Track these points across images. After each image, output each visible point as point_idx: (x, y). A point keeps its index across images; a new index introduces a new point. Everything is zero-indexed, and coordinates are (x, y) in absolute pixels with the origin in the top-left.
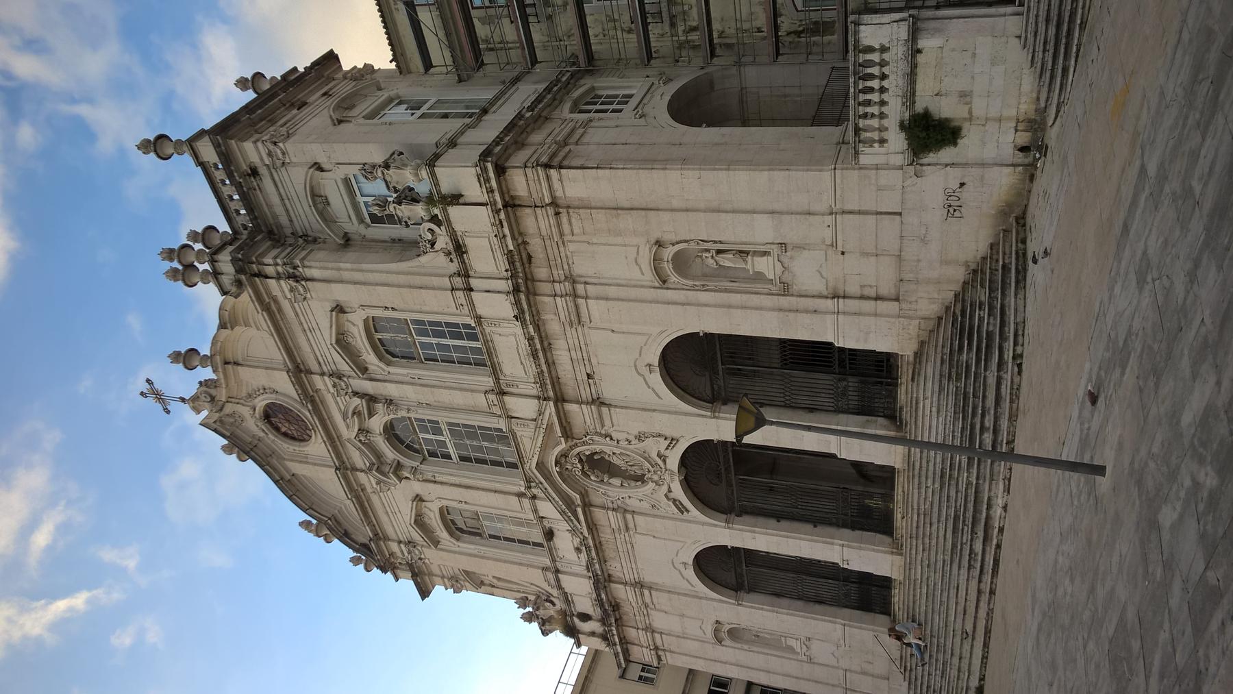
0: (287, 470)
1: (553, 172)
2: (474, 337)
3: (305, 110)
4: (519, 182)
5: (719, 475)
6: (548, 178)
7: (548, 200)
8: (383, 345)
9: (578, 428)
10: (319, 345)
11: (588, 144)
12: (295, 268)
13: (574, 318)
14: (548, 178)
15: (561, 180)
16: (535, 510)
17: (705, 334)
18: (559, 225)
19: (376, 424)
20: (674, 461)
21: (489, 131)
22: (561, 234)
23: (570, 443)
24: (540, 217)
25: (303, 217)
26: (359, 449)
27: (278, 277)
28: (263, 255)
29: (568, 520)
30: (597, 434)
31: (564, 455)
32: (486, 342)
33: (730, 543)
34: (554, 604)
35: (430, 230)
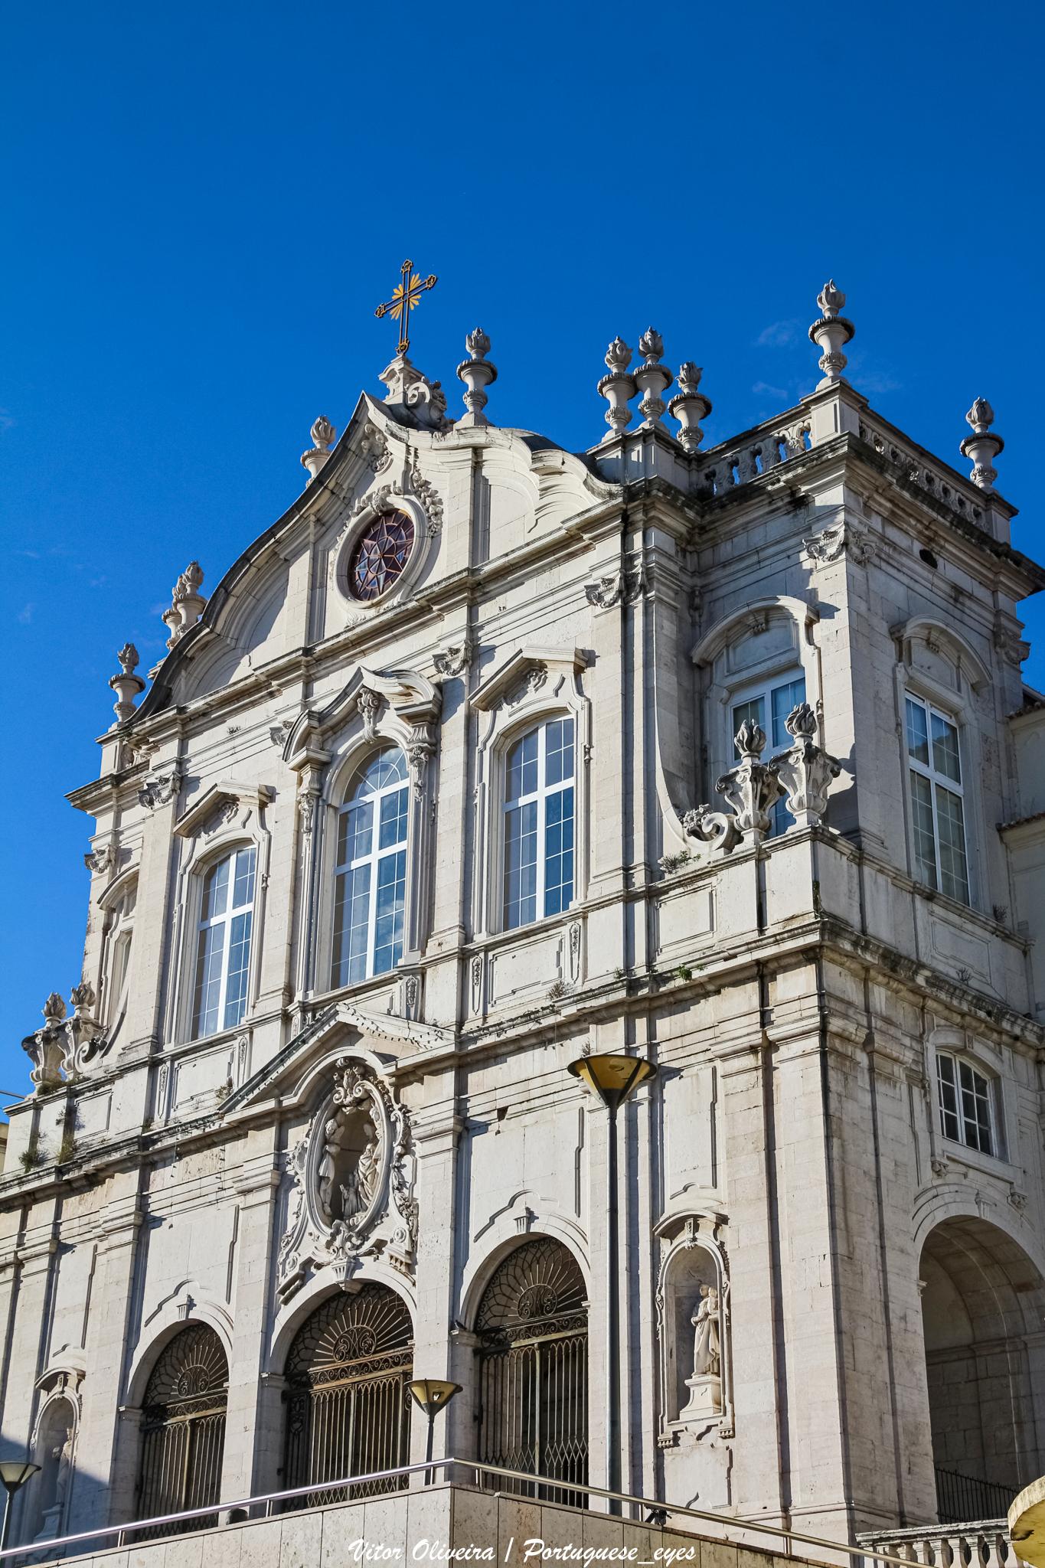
0: (297, 554)
1: (814, 1042)
2: (551, 908)
3: (921, 569)
4: (796, 987)
5: (353, 1354)
6: (805, 1034)
7: (773, 1034)
8: (526, 737)
9: (412, 1094)
10: (516, 626)
11: (873, 1091)
14: (805, 1034)
15: (804, 1055)
16: (263, 1021)
17: (921, 1278)
18: (737, 1053)
19: (391, 725)
20: (372, 1270)
21: (886, 918)
22: (724, 1057)
23: (387, 1081)
24: (745, 1020)
25: (732, 587)
26: (345, 694)
27: (627, 560)
29: (251, 1085)
30: (407, 1129)
31: (368, 1072)
32: (545, 928)
34: (87, 1059)
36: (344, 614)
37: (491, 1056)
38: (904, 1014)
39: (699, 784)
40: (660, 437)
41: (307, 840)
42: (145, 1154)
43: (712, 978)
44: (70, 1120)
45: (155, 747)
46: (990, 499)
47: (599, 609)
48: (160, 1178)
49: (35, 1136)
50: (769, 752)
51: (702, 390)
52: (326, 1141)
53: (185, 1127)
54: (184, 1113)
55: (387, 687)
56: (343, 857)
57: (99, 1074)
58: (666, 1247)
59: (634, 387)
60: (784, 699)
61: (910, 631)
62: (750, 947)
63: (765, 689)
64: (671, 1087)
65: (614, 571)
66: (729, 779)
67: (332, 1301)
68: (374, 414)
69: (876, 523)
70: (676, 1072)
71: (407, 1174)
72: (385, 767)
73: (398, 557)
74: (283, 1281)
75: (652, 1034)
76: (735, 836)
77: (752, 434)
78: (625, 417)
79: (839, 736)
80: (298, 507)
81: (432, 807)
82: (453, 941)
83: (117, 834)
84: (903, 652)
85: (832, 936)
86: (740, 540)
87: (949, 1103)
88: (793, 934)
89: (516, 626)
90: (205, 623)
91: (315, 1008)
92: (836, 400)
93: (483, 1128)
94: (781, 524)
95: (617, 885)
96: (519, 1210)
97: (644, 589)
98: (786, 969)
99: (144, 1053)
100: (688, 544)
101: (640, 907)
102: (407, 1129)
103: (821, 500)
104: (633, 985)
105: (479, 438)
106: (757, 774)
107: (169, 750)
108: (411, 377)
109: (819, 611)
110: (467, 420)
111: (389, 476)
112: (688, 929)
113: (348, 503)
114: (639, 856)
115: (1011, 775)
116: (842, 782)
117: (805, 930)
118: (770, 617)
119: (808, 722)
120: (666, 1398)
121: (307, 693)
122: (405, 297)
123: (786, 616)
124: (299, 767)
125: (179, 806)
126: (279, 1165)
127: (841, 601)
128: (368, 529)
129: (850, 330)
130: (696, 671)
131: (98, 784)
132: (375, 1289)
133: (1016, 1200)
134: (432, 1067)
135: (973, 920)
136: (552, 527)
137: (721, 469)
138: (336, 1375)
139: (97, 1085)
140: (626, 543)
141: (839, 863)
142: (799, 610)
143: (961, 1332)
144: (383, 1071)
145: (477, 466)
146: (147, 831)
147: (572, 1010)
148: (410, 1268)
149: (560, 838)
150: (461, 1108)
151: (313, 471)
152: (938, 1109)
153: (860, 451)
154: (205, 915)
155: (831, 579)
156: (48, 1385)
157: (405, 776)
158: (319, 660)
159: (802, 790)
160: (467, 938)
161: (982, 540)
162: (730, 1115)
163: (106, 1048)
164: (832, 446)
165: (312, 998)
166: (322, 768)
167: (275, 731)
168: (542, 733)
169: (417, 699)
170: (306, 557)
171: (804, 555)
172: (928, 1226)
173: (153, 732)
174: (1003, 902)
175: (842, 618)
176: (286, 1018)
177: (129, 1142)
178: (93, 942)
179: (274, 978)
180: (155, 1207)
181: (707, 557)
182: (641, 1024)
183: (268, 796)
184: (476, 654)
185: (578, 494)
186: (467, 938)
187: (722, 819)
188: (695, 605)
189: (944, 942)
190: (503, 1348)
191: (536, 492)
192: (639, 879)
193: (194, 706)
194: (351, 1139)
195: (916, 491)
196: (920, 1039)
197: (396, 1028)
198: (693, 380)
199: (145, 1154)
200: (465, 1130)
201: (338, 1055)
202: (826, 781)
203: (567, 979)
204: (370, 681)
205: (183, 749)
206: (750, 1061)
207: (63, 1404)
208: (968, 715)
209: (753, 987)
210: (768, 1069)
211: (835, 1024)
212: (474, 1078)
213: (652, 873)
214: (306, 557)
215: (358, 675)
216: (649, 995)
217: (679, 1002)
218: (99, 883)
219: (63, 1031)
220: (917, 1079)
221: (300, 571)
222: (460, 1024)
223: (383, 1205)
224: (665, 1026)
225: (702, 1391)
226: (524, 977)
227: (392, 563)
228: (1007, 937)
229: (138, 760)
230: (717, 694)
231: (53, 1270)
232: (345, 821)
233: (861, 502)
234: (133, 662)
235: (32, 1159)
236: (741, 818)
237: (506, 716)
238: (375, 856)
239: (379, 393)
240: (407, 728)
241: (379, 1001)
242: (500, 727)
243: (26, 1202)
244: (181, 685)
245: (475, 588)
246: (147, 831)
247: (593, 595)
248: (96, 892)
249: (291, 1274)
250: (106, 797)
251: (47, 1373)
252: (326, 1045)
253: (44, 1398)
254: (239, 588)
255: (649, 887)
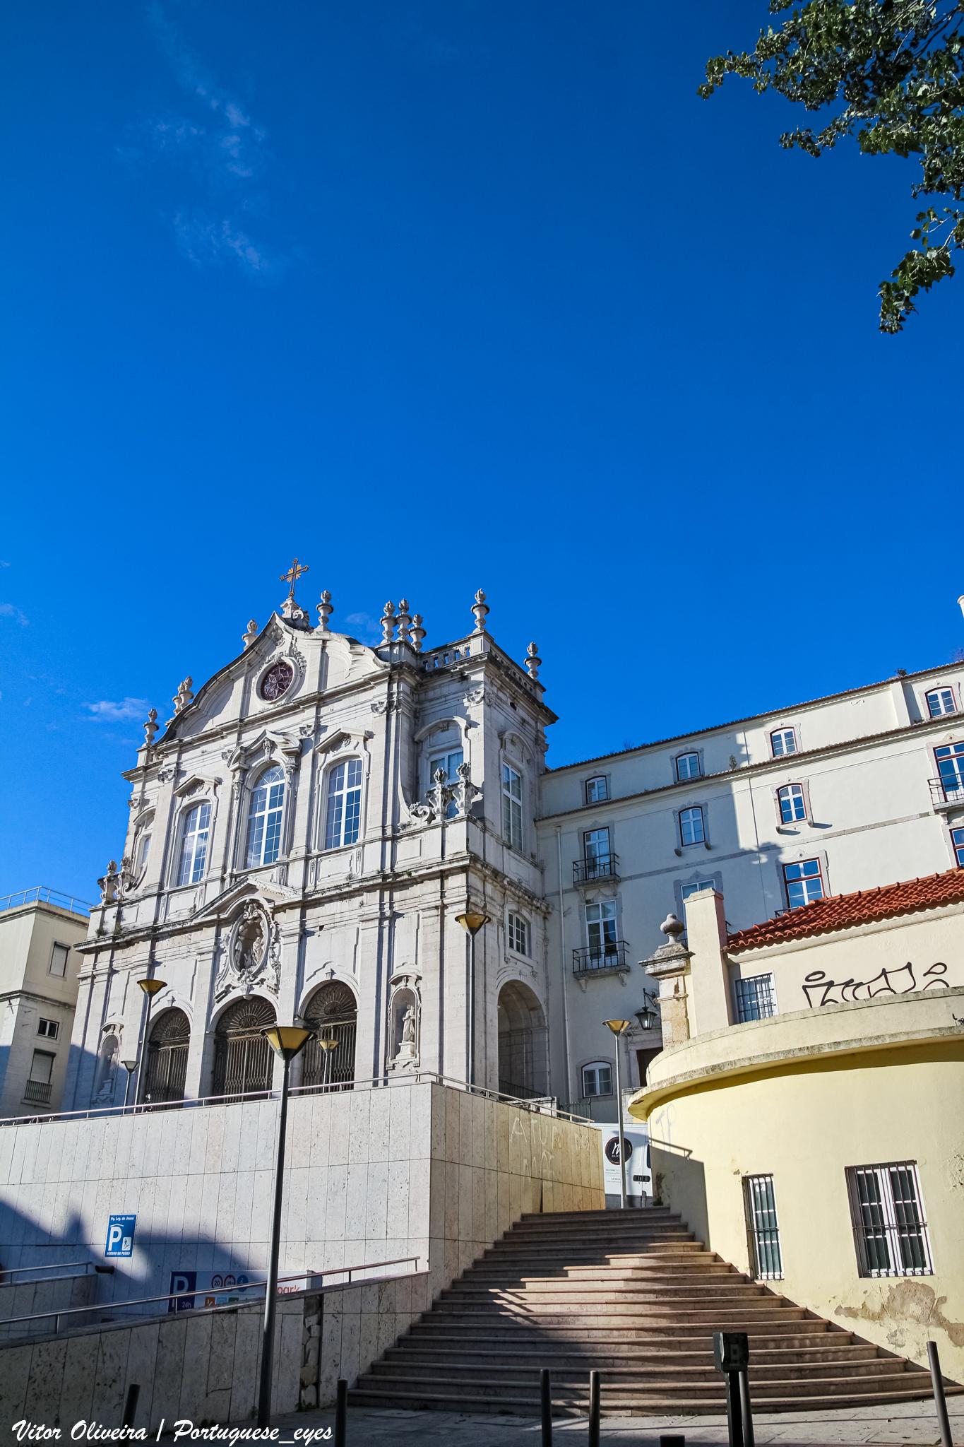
0: (238, 678)
3: (510, 710)
4: (457, 883)
7: (446, 902)
10: (337, 718)
12: (397, 708)
13: (365, 917)
19: (278, 755)
21: (495, 855)
26: (258, 740)
27: (390, 695)
28: (406, 682)
29: (206, 908)
30: (277, 932)
31: (260, 906)
32: (345, 850)
33: (192, 1035)
35: (915, 267)
36: (258, 706)
37: (318, 903)
38: (498, 896)
39: (415, 793)
40: (406, 643)
41: (236, 803)
42: (154, 934)
43: (420, 876)
44: (119, 917)
45: (167, 756)
46: (536, 684)
47: (376, 714)
48: (160, 945)
49: (102, 922)
50: (448, 782)
51: (422, 626)
52: (239, 934)
53: (174, 924)
54: (173, 918)
55: (278, 739)
56: (251, 811)
57: (134, 898)
58: (394, 989)
59: (396, 622)
60: (454, 760)
61: (507, 736)
62: (438, 864)
63: (445, 755)
64: (399, 921)
65: (384, 699)
66: (431, 792)
67: (239, 1003)
68: (278, 621)
69: (495, 689)
70: (401, 915)
71: (276, 951)
72: (273, 774)
73: (285, 684)
74: (217, 993)
75: (391, 898)
76: (432, 817)
77: (445, 647)
78: (390, 634)
79: (477, 778)
80: (241, 657)
81: (295, 793)
82: (302, 852)
83: (143, 792)
84: (503, 745)
85: (474, 863)
86: (438, 691)
87: (511, 934)
88: (458, 860)
89: (337, 718)
90: (194, 704)
91: (236, 876)
92: (482, 638)
93: (312, 933)
94: (455, 686)
95: (379, 834)
96: (328, 969)
97: (397, 708)
98: (453, 874)
99: (155, 890)
100: (415, 690)
101: (389, 844)
102: (277, 932)
103: (473, 678)
104: (385, 877)
105: (326, 636)
106: (444, 791)
107: (173, 758)
108: (295, 607)
109: (471, 724)
110: (320, 628)
111: (281, 650)
112: (409, 855)
113: (263, 658)
114: (389, 822)
115: (540, 798)
116: (478, 797)
117: (463, 859)
118: (449, 724)
119: (466, 770)
120: (390, 1050)
121: (239, 738)
122: (294, 573)
123: (457, 725)
124: (235, 770)
125: (176, 783)
126: (217, 943)
127: (481, 721)
128: (272, 670)
129: (488, 609)
130: (416, 744)
131: (137, 770)
132: (260, 999)
133: (534, 974)
134: (291, 906)
135: (524, 858)
136: (357, 677)
137: (430, 660)
138: (238, 1034)
139: (132, 902)
140: (390, 688)
141: (476, 831)
142: (462, 723)
143: (507, 1027)
144: (267, 906)
145: (324, 648)
146: (159, 794)
147: (357, 886)
148: (276, 991)
149: (353, 811)
150: (303, 924)
151: (247, 642)
152: (508, 937)
153: (492, 660)
154: (185, 832)
155: (476, 711)
156: (107, 1029)
157: (283, 778)
158: (246, 725)
159: (463, 799)
160: (309, 851)
161: (533, 700)
162: (425, 935)
163: (136, 886)
164: (480, 656)
165: (235, 872)
166: (244, 771)
167: (224, 754)
168: (347, 765)
169: (291, 745)
170: (243, 679)
171: (465, 700)
172: (502, 984)
173: (166, 749)
174: (535, 851)
175: (481, 728)
176: (223, 880)
177: (147, 928)
178: (130, 839)
179: (218, 862)
180: (158, 957)
181: (423, 697)
182: (387, 894)
183: (218, 782)
184: (319, 729)
185: (369, 664)
186: (309, 851)
187: (427, 809)
188: (417, 717)
189: (515, 868)
190: (317, 1027)
191: (350, 662)
192: (389, 832)
193: (186, 739)
194: (251, 933)
195: (512, 679)
196: (503, 906)
197: (275, 888)
198: (419, 622)
199: (154, 934)
200: (304, 934)
201: (247, 898)
202: (472, 796)
203: (354, 872)
204: (269, 736)
205: (179, 758)
206: (435, 912)
207: (113, 1038)
208: (525, 773)
209: (438, 881)
210: (443, 916)
211: (473, 899)
212: (308, 912)
213: (395, 830)
214: (243, 679)
215: (264, 733)
216: (391, 882)
217: (404, 886)
218: (134, 813)
219: (116, 879)
220: (501, 923)
221: (239, 685)
222: (304, 888)
223: (265, 963)
224: (397, 895)
225: (406, 1048)
226: (334, 870)
227: (282, 686)
228: (536, 866)
229: (155, 760)
230: (425, 755)
231: (109, 981)
232: (253, 796)
233: (490, 681)
234: (155, 717)
235: (101, 932)
236: (435, 809)
237: (331, 756)
238: (267, 812)
239: (281, 612)
240: (286, 758)
241: (266, 875)
242: (328, 761)
243: (97, 950)
244: (181, 730)
245: (320, 700)
246: (159, 794)
247: (374, 708)
248: (132, 818)
249: (221, 990)
250: (140, 775)
251: (106, 1024)
252: (241, 893)
253: (105, 1035)
254: (210, 690)
255: (393, 835)
